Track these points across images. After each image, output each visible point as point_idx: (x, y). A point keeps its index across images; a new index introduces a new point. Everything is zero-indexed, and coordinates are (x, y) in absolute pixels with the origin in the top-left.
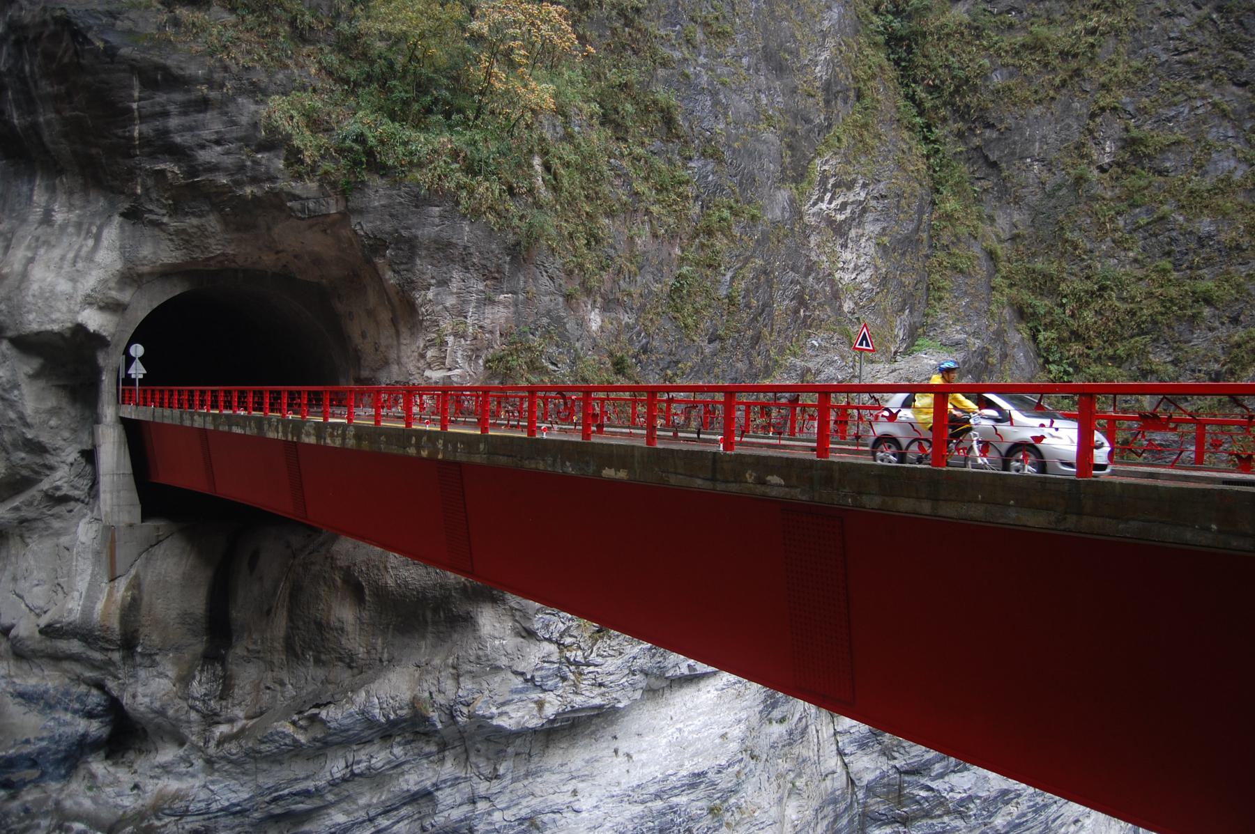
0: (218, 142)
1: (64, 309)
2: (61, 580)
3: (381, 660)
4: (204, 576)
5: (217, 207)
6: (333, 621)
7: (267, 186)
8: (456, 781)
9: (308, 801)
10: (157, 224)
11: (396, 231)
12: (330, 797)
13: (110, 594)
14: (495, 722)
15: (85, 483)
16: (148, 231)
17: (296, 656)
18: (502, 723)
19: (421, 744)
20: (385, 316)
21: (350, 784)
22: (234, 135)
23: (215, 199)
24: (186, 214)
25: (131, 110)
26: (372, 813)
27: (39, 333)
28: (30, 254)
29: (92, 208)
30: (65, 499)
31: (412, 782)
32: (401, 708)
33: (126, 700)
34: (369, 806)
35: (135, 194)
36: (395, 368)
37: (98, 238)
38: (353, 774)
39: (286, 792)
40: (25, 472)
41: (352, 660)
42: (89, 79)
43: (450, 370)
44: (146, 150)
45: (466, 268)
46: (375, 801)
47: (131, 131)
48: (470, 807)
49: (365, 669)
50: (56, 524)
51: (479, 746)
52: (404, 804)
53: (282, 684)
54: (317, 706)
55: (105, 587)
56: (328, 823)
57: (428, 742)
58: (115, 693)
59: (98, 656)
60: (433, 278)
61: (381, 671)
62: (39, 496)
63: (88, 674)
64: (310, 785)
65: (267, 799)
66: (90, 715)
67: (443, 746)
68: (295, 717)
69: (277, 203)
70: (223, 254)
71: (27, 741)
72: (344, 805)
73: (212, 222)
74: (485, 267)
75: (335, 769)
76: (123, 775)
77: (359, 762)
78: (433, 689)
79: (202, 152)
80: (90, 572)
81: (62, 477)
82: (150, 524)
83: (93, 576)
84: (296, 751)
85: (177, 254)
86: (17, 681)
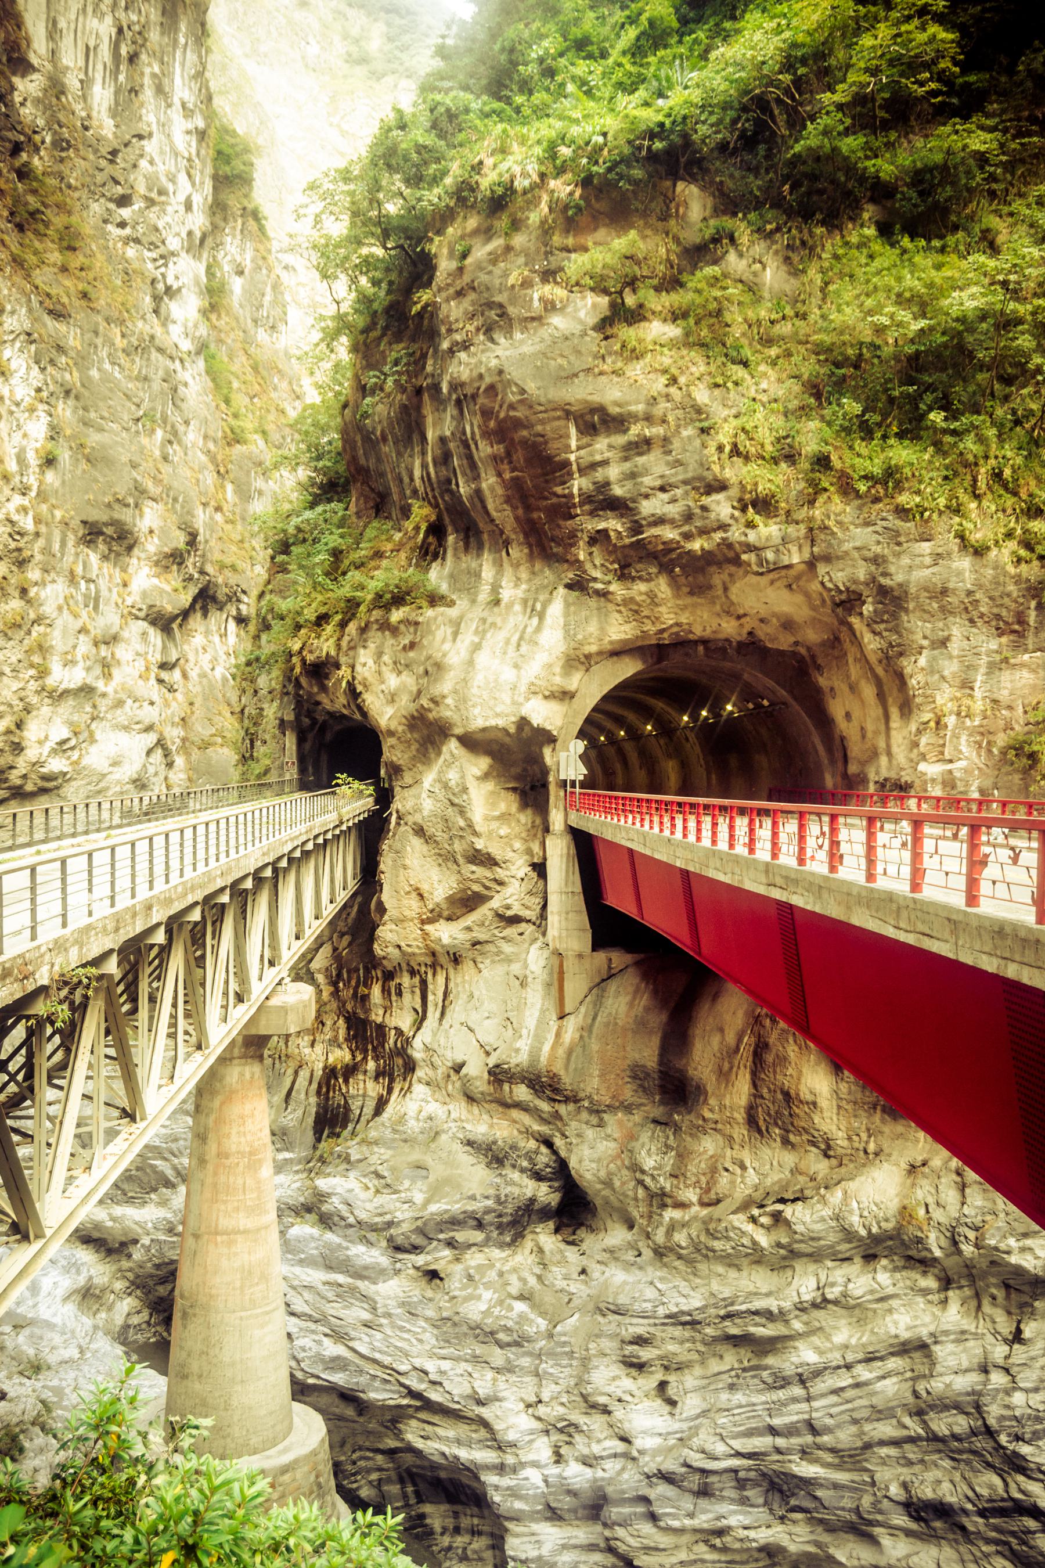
0: (662, 489)
1: (508, 701)
2: (510, 1014)
3: (866, 1152)
4: (658, 1020)
5: (666, 568)
6: (805, 1095)
7: (718, 536)
8: (962, 1336)
9: (770, 1325)
10: (604, 595)
11: (874, 580)
12: (797, 1325)
13: (558, 1035)
14: (1013, 1259)
15: (536, 902)
16: (593, 602)
17: (760, 1131)
18: (1025, 1264)
19: (915, 1275)
20: (869, 691)
21: (822, 1312)
22: (681, 477)
23: (666, 559)
24: (633, 579)
25: (567, 464)
26: (850, 1357)
27: (484, 730)
28: (477, 640)
29: (537, 581)
30: (515, 920)
31: (902, 1326)
32: (887, 1220)
33: (573, 1164)
34: (847, 1347)
35: (578, 561)
36: (884, 760)
37: (541, 616)
38: (825, 1300)
39: (743, 1307)
40: (476, 888)
41: (829, 1147)
42: (525, 433)
43: (951, 761)
44: (587, 507)
45: (971, 621)
46: (853, 1341)
47: (570, 488)
48: (981, 1377)
49: (844, 1160)
50: (507, 948)
51: (994, 1291)
52: (892, 1354)
53: (743, 1167)
54: (782, 1201)
55: (554, 1025)
56: (795, 1359)
57: (925, 1273)
58: (563, 1154)
59: (545, 1106)
60: (925, 637)
61: (864, 1165)
62: (490, 915)
63: (536, 1127)
64: (773, 1304)
65: (722, 1312)
66: (538, 1176)
67: (947, 1283)
68: (756, 1212)
69: (728, 557)
70: (677, 624)
71: (473, 1198)
72: (815, 1340)
73: (662, 586)
74: (998, 617)
75: (803, 1290)
76: (571, 1253)
77: (833, 1285)
78: (930, 1200)
79: (645, 503)
80: (539, 1006)
81: (514, 895)
82: (601, 956)
83: (543, 1011)
84: (757, 1257)
85: (627, 627)
86: (468, 1127)
